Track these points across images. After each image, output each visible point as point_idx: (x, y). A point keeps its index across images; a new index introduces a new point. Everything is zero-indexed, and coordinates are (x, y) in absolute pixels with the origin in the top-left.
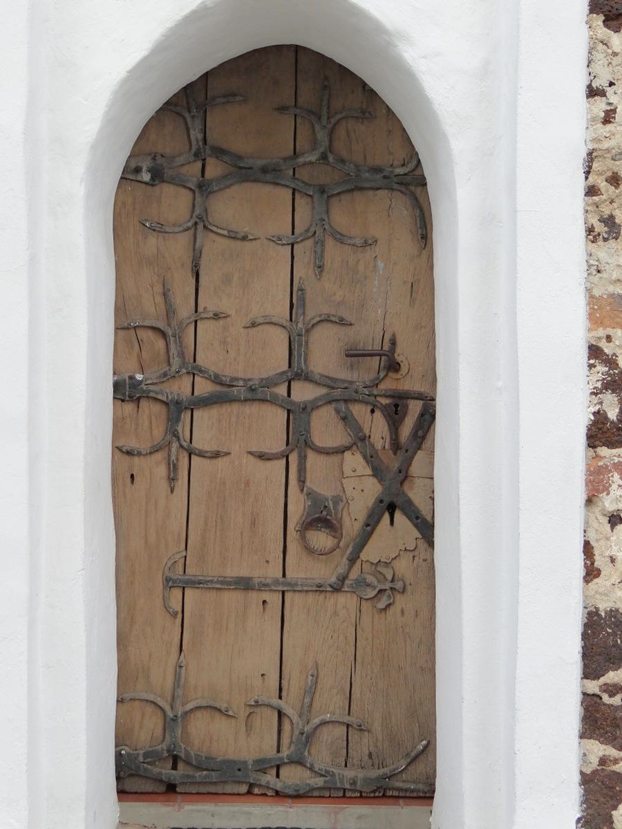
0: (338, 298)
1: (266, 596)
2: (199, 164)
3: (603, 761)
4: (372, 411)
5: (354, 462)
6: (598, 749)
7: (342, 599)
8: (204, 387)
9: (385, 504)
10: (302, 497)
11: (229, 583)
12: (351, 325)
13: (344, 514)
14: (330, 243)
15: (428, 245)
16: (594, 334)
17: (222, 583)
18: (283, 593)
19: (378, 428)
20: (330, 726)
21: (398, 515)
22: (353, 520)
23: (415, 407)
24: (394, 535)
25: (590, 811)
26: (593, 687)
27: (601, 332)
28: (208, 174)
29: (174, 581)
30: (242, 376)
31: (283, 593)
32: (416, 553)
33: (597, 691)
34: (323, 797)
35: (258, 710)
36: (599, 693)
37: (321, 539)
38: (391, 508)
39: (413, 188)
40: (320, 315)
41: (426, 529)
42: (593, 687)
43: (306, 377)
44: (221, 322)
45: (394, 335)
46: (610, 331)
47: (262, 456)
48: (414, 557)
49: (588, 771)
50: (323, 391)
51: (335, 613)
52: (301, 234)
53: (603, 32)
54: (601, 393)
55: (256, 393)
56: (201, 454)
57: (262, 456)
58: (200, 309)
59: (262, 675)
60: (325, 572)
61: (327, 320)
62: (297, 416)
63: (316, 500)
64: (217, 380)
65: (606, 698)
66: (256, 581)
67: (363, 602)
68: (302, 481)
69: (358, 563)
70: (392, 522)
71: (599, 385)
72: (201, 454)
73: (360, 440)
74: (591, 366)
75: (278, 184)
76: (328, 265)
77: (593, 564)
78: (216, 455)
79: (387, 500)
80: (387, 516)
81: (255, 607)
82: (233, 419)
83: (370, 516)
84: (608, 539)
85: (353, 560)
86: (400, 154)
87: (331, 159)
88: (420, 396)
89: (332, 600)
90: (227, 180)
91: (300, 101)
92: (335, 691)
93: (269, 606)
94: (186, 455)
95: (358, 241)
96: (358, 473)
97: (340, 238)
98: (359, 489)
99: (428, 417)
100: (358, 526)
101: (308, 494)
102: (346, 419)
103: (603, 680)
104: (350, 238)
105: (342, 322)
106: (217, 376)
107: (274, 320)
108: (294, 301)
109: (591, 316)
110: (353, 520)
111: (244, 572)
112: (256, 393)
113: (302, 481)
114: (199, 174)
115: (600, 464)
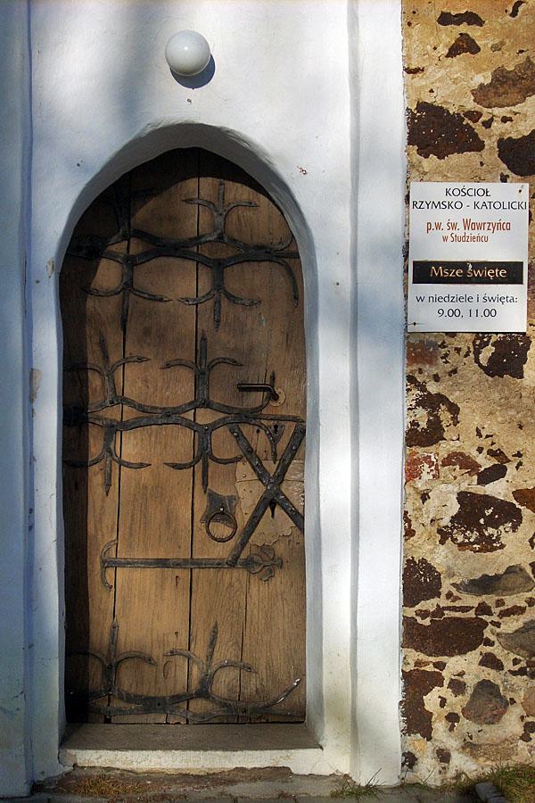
0: (232, 346)
1: (178, 572)
2: (127, 242)
3: (418, 663)
4: (258, 431)
5: (244, 469)
6: (415, 655)
7: (235, 573)
8: (129, 413)
9: (267, 501)
10: (205, 498)
11: (151, 564)
12: (242, 365)
13: (237, 510)
14: (225, 303)
15: (300, 305)
16: (410, 368)
17: (145, 563)
18: (191, 569)
19: (260, 442)
20: (226, 670)
21: (277, 509)
22: (243, 514)
23: (289, 428)
24: (278, 522)
25: (408, 697)
26: (411, 612)
27: (415, 367)
28: (132, 252)
29: (109, 563)
30: (160, 406)
31: (191, 569)
32: (291, 538)
33: (414, 615)
34: (223, 723)
35: (172, 659)
36: (414, 616)
37: (221, 530)
38: (273, 504)
39: (287, 260)
40: (218, 359)
41: (298, 518)
42: (411, 612)
43: (207, 404)
44: (143, 364)
45: (273, 373)
46: (420, 366)
47: (176, 466)
48: (289, 541)
49: (407, 669)
50: (222, 415)
51: (231, 585)
52: (204, 297)
53: (416, 157)
54: (415, 408)
55: (170, 416)
56: (129, 465)
57: (176, 466)
58: (127, 355)
59: (176, 633)
60: (222, 552)
61: (224, 361)
62: (204, 433)
63: (213, 498)
64: (141, 408)
65: (419, 620)
66: (171, 562)
67: (252, 575)
68: (205, 484)
69: (248, 546)
70: (273, 516)
71: (414, 403)
72: (129, 465)
73: (249, 453)
74: (408, 390)
75: (186, 258)
76: (223, 319)
77: (410, 526)
78: (141, 465)
79: (270, 498)
80: (269, 510)
81: (170, 583)
82: (153, 439)
83: (256, 510)
84: (420, 509)
85: (243, 544)
86: (150, 747)
87: (226, 240)
88: (294, 419)
89: (228, 576)
90: (147, 256)
91: (202, 193)
92: (231, 643)
93: (180, 582)
94: (117, 465)
95: (247, 303)
96: (247, 478)
97: (232, 298)
98: (246, 491)
99: (300, 434)
100: (247, 518)
101: (210, 495)
102: (239, 437)
103: (417, 607)
104: (241, 299)
105: (234, 363)
106: (140, 406)
107: (183, 362)
108: (198, 348)
109: (409, 356)
110: (243, 514)
111: (162, 555)
112: (170, 416)
113: (205, 484)
114: (126, 252)
115: (415, 457)
